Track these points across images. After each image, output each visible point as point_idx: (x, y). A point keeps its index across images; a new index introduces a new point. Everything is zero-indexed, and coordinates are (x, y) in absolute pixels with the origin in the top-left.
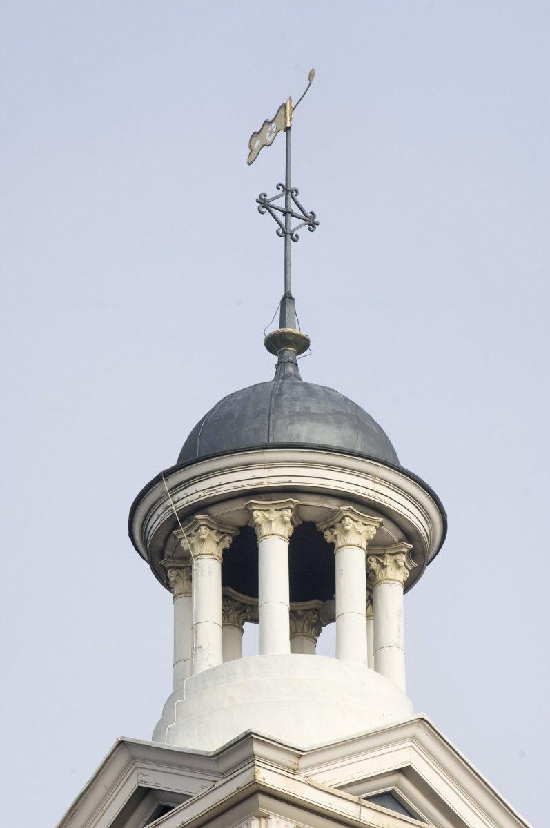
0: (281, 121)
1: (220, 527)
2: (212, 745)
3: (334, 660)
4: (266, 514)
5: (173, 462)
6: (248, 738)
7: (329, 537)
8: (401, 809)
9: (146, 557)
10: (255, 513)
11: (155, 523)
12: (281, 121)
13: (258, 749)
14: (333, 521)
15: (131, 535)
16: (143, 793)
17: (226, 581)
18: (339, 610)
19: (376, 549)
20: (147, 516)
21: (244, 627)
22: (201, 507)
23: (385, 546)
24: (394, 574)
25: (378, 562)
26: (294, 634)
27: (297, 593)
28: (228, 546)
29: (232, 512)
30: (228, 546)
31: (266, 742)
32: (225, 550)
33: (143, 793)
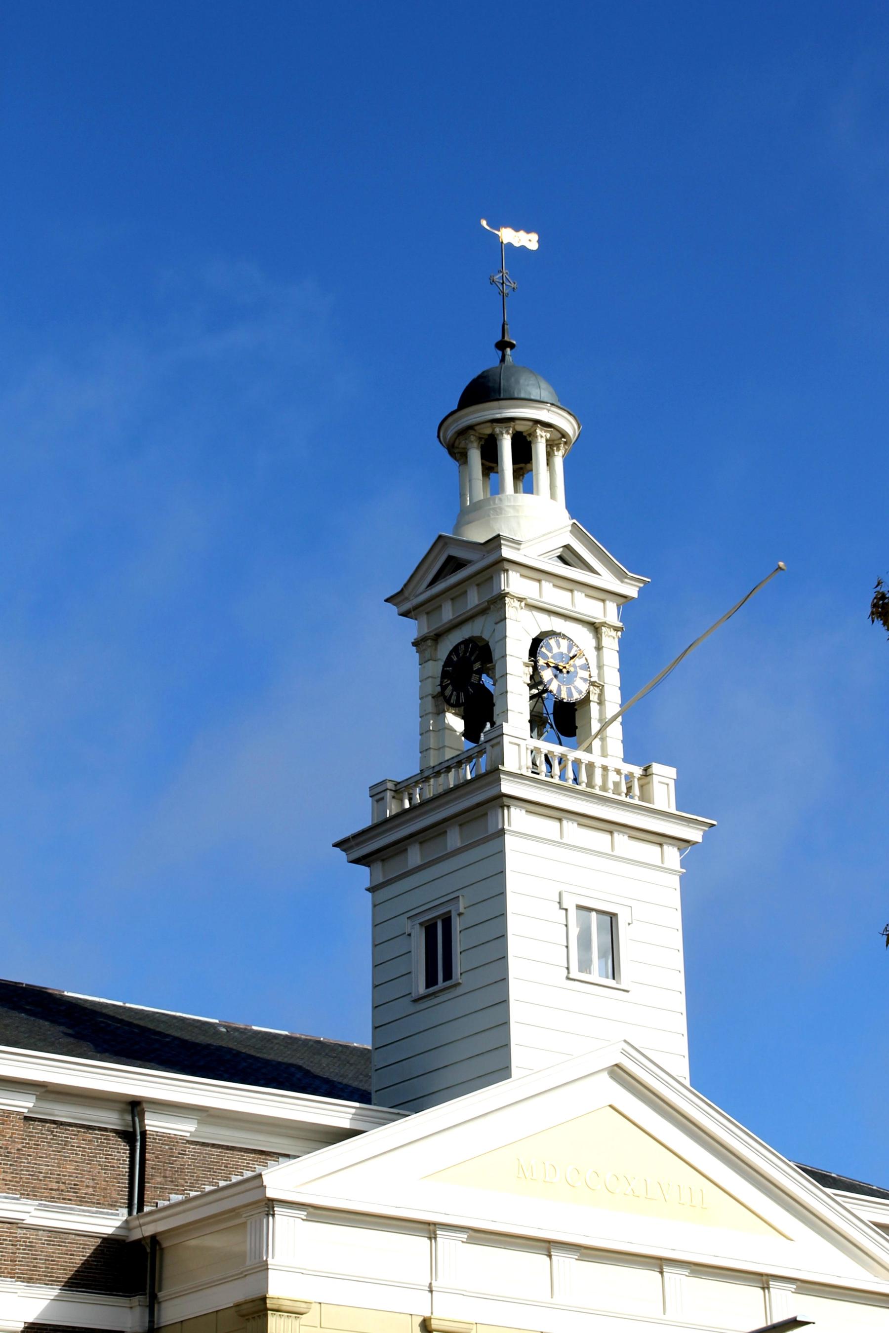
3: (589, 975)
4: (501, 429)
5: (456, 408)
7: (529, 439)
8: (583, 566)
9: (445, 446)
10: (496, 429)
11: (450, 433)
15: (439, 437)
16: (450, 558)
17: (482, 458)
18: (531, 641)
19: (551, 446)
20: (446, 431)
21: (490, 476)
22: (471, 428)
23: (234, 1211)
25: (289, 1055)
26: (483, 475)
27: (515, 461)
28: (483, 443)
30: (483, 443)
32: (482, 445)
33: (450, 558)
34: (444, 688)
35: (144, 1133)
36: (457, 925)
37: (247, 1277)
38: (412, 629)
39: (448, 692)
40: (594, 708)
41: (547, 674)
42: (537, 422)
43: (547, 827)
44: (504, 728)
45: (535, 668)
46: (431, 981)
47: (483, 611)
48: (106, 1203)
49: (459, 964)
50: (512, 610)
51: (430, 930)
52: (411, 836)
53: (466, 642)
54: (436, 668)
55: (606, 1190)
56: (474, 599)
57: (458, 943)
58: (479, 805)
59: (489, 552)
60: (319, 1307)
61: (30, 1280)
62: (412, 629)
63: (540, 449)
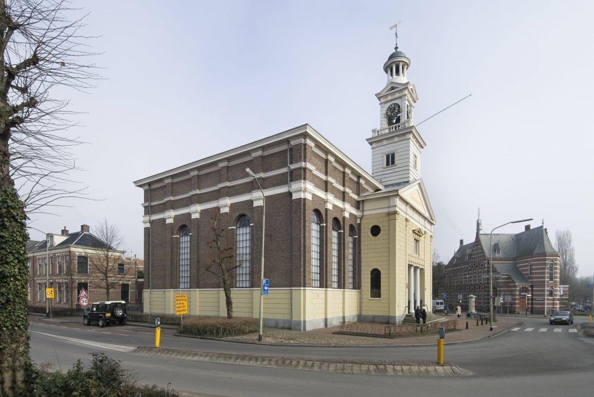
0: (396, 26)
2: (404, 83)
12: (396, 26)
29: (397, 63)
34: (387, 113)
36: (396, 156)
39: (388, 113)
47: (400, 97)
49: (396, 162)
53: (394, 104)
54: (385, 109)
56: (397, 95)
60: (341, 296)
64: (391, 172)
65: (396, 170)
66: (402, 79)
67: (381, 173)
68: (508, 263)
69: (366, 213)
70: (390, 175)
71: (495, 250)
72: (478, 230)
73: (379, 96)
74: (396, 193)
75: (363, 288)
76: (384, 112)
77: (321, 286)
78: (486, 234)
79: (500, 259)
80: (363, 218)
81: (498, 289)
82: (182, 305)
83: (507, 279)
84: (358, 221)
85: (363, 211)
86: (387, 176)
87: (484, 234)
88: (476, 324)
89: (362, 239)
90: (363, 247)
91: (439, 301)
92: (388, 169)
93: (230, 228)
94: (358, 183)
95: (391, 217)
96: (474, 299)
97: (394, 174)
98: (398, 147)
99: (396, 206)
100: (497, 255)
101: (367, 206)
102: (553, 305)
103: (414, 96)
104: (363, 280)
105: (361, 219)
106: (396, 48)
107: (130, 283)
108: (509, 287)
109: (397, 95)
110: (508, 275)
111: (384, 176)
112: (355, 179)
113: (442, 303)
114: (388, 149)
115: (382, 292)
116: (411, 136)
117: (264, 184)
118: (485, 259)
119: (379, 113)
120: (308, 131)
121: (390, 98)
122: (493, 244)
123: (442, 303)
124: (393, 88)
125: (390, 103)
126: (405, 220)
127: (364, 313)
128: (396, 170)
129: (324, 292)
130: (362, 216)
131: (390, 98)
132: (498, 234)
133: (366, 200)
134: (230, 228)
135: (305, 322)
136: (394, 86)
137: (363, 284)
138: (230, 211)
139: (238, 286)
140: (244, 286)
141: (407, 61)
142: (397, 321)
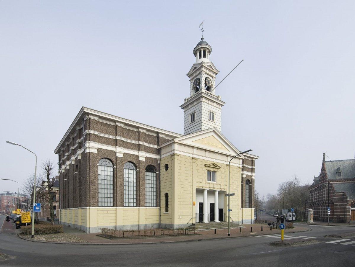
1: (199, 50)
6: (202, 62)
13: (84, 108)
14: (206, 50)
22: (198, 49)
24: (209, 54)
31: (84, 107)
34: (193, 85)
35: (159, 137)
36: (195, 114)
37: (230, 216)
38: (189, 79)
40: (212, 88)
41: (207, 82)
42: (207, 48)
43: (207, 101)
44: (183, 120)
45: (206, 81)
46: (192, 121)
47: (199, 74)
48: (155, 144)
49: (195, 119)
50: (203, 73)
51: (191, 115)
52: (190, 104)
53: (197, 79)
55: (36, 155)
56: (198, 72)
57: (195, 116)
58: (199, 98)
59: (201, 64)
60: (250, 211)
61: (146, 152)
62: (189, 79)
63: (207, 53)
64: (192, 126)
65: (195, 124)
66: (206, 61)
67: (188, 128)
68: (347, 183)
69: (162, 156)
70: (193, 128)
71: (337, 173)
72: (324, 158)
73: (189, 75)
74: (173, 141)
75: (161, 206)
76: (192, 86)
77: (136, 206)
78: (331, 161)
79: (340, 180)
80: (162, 160)
81: (334, 204)
82: (26, 218)
83: (343, 195)
84: (159, 162)
85: (161, 155)
86: (191, 129)
87: (329, 161)
88: (214, 233)
89: (161, 174)
90: (161, 179)
91: (291, 214)
92: (192, 124)
93: (77, 173)
94: (158, 137)
95: (173, 157)
96: (312, 212)
97: (194, 127)
98: (196, 109)
99: (174, 150)
100: (338, 177)
101: (163, 152)
102: (345, 216)
103: (214, 70)
104: (161, 201)
105: (160, 160)
106: (202, 39)
107: (56, 205)
108: (343, 202)
109: (198, 72)
110: (343, 193)
111: (189, 130)
112: (155, 135)
113: (293, 216)
114: (191, 111)
115: (169, 208)
116: (203, 99)
117: (125, 145)
118: (326, 181)
119: (189, 86)
120: (85, 111)
121: (194, 75)
122: (336, 168)
123: (293, 216)
124: (195, 68)
125: (195, 79)
126: (191, 159)
127: (162, 222)
128: (195, 124)
129: (251, 210)
130: (161, 159)
131: (194, 75)
132: (342, 160)
133: (161, 148)
134: (77, 173)
135: (89, 228)
136: (196, 66)
137: (161, 204)
138: (75, 163)
139: (124, 205)
140: (132, 206)
141: (209, 48)
142: (175, 228)
